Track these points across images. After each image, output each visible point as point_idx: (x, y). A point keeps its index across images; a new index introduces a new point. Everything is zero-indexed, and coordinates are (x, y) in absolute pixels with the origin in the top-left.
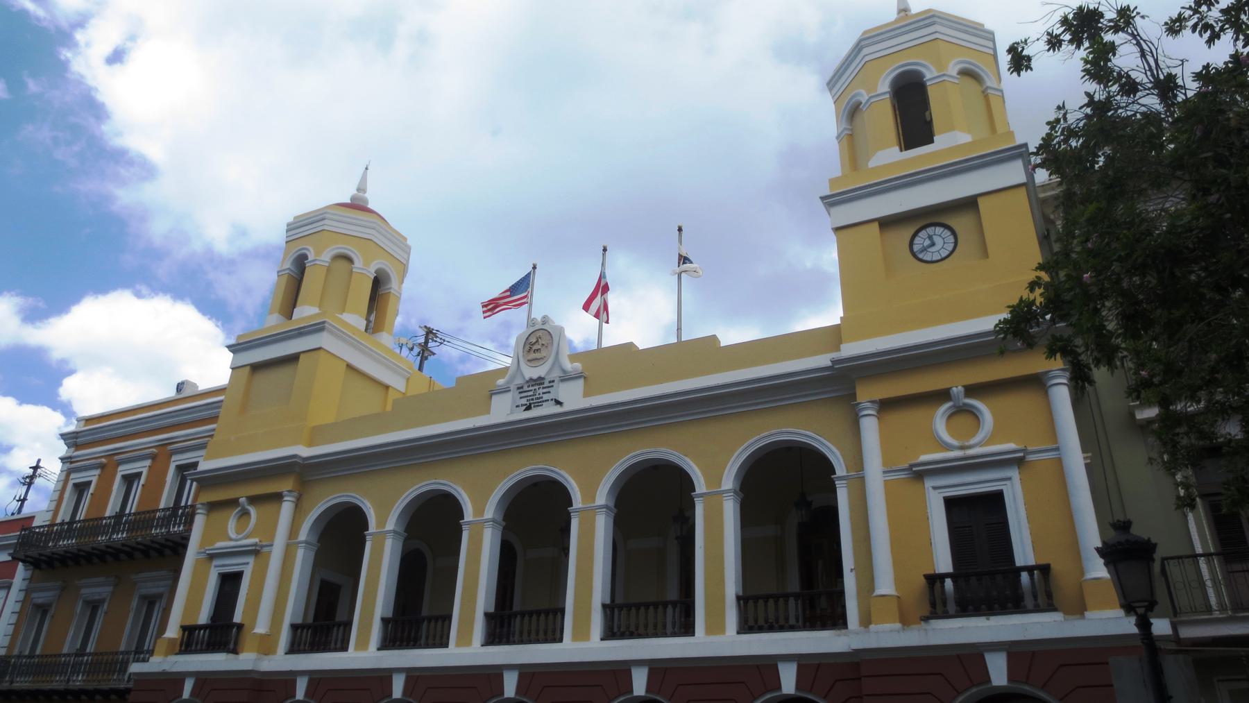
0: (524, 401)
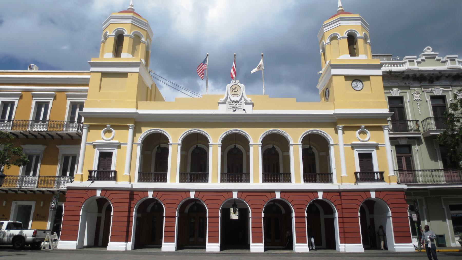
0: (231, 107)
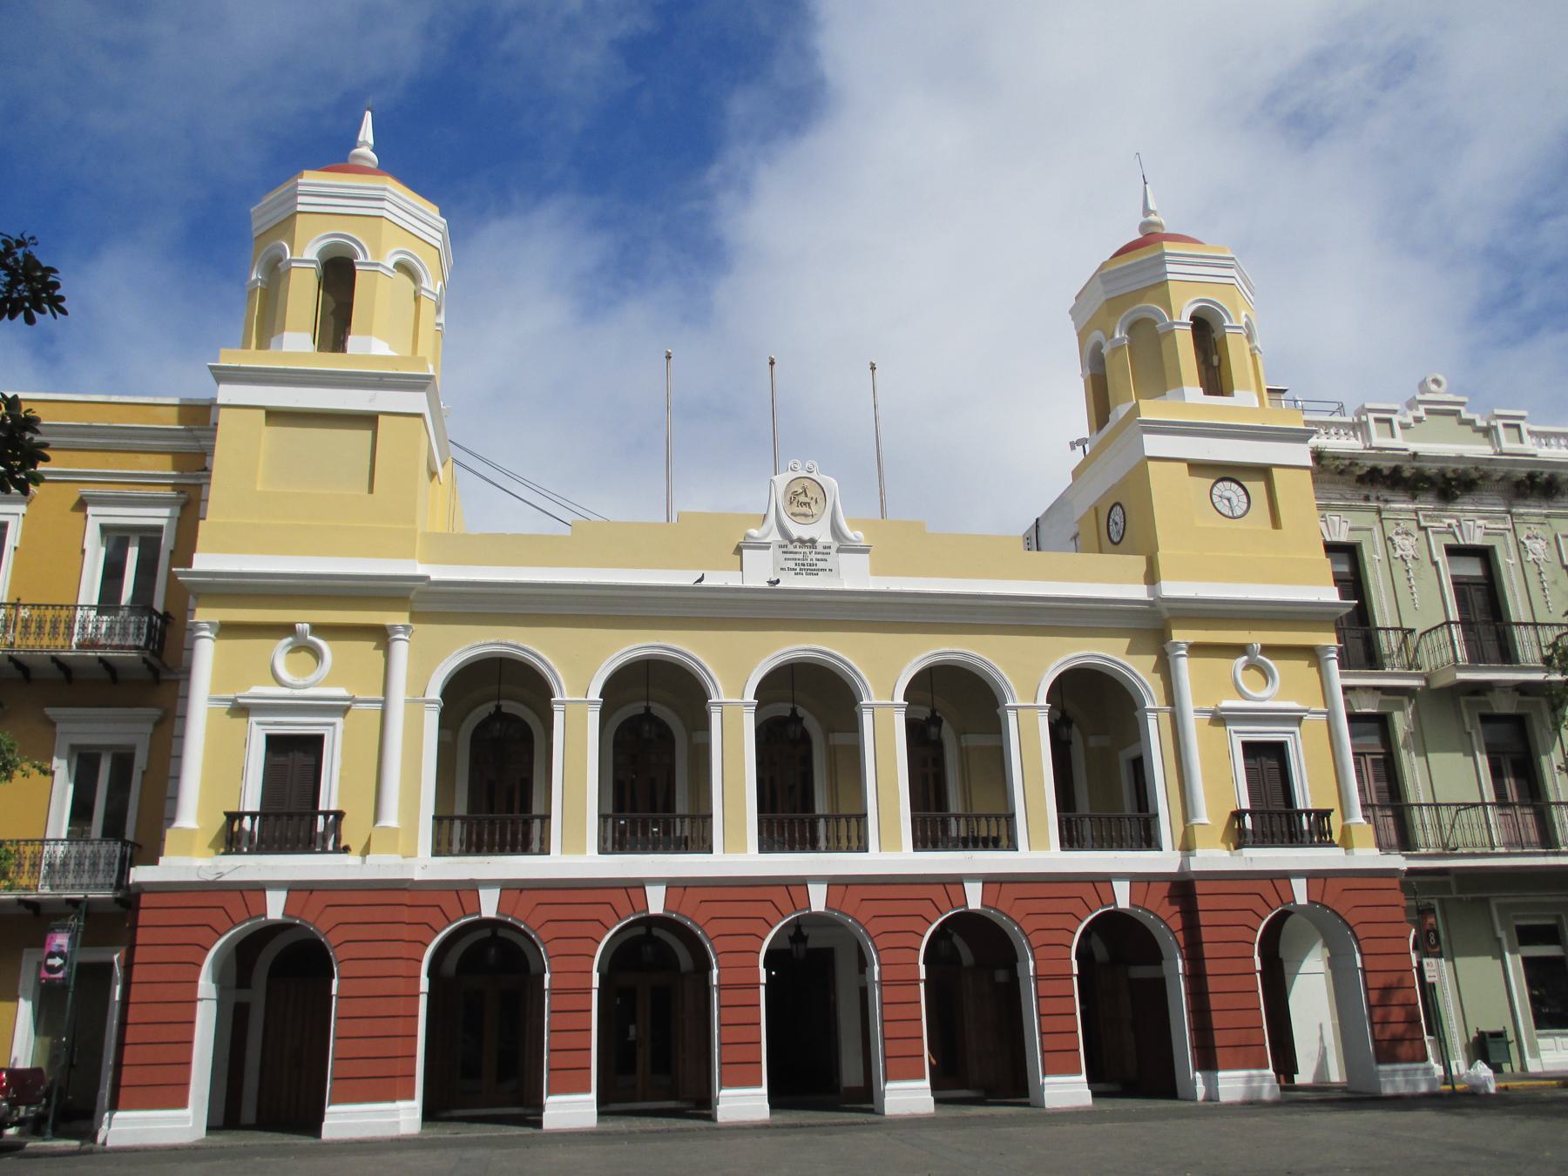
0: (791, 564)
